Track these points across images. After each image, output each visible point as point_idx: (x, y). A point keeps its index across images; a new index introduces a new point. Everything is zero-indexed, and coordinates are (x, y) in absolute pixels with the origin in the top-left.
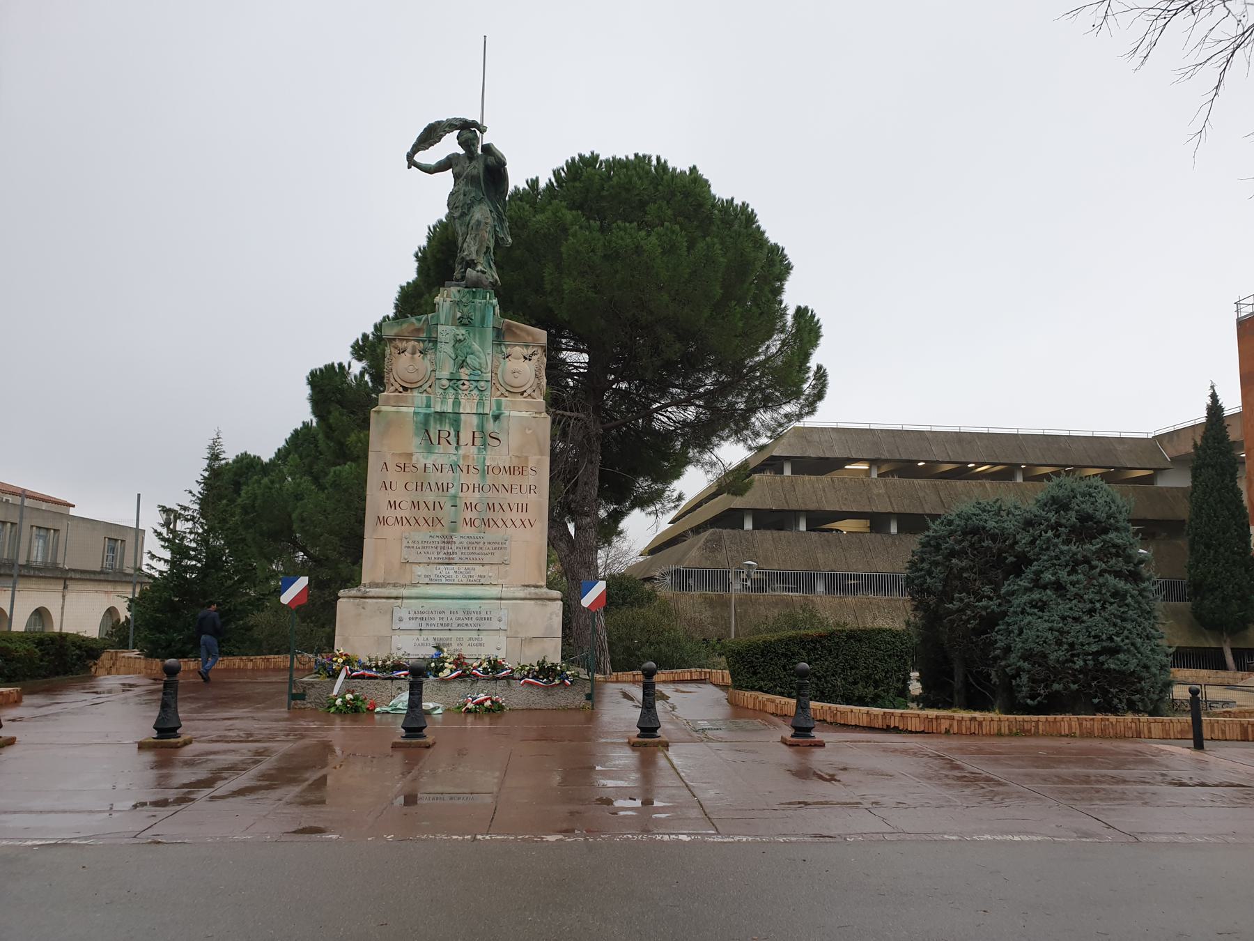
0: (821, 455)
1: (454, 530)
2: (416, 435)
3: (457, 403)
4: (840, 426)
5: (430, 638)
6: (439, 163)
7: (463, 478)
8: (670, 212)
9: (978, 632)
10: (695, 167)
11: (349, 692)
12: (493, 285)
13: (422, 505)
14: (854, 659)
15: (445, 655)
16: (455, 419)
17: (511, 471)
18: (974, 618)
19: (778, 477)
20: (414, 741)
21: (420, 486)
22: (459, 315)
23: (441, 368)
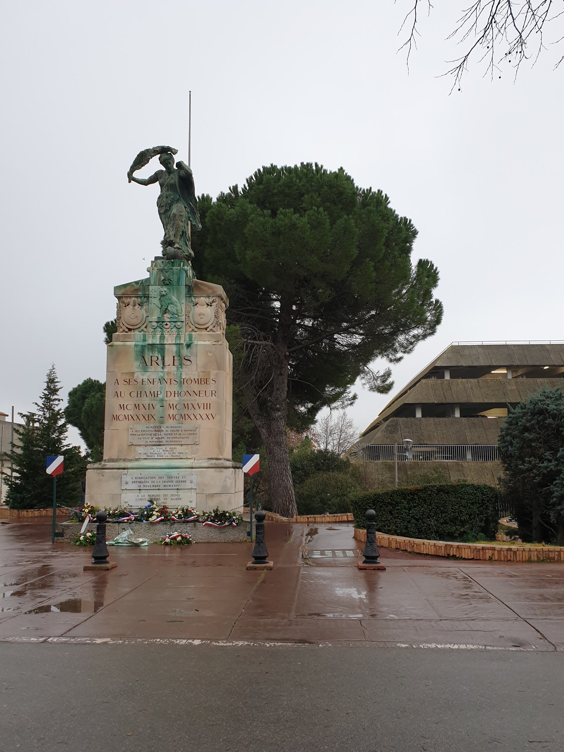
0: (471, 364)
1: (162, 422)
2: (136, 359)
3: (162, 337)
4: (485, 343)
5: (146, 495)
6: (150, 177)
7: (168, 388)
8: (319, 199)
9: (541, 485)
10: (342, 168)
11: (89, 531)
12: (188, 257)
13: (141, 407)
14: (444, 506)
15: (154, 506)
16: (161, 348)
17: (198, 381)
18: (538, 475)
19: (439, 381)
20: (98, 565)
21: (140, 394)
22: (163, 278)
23: (152, 315)
